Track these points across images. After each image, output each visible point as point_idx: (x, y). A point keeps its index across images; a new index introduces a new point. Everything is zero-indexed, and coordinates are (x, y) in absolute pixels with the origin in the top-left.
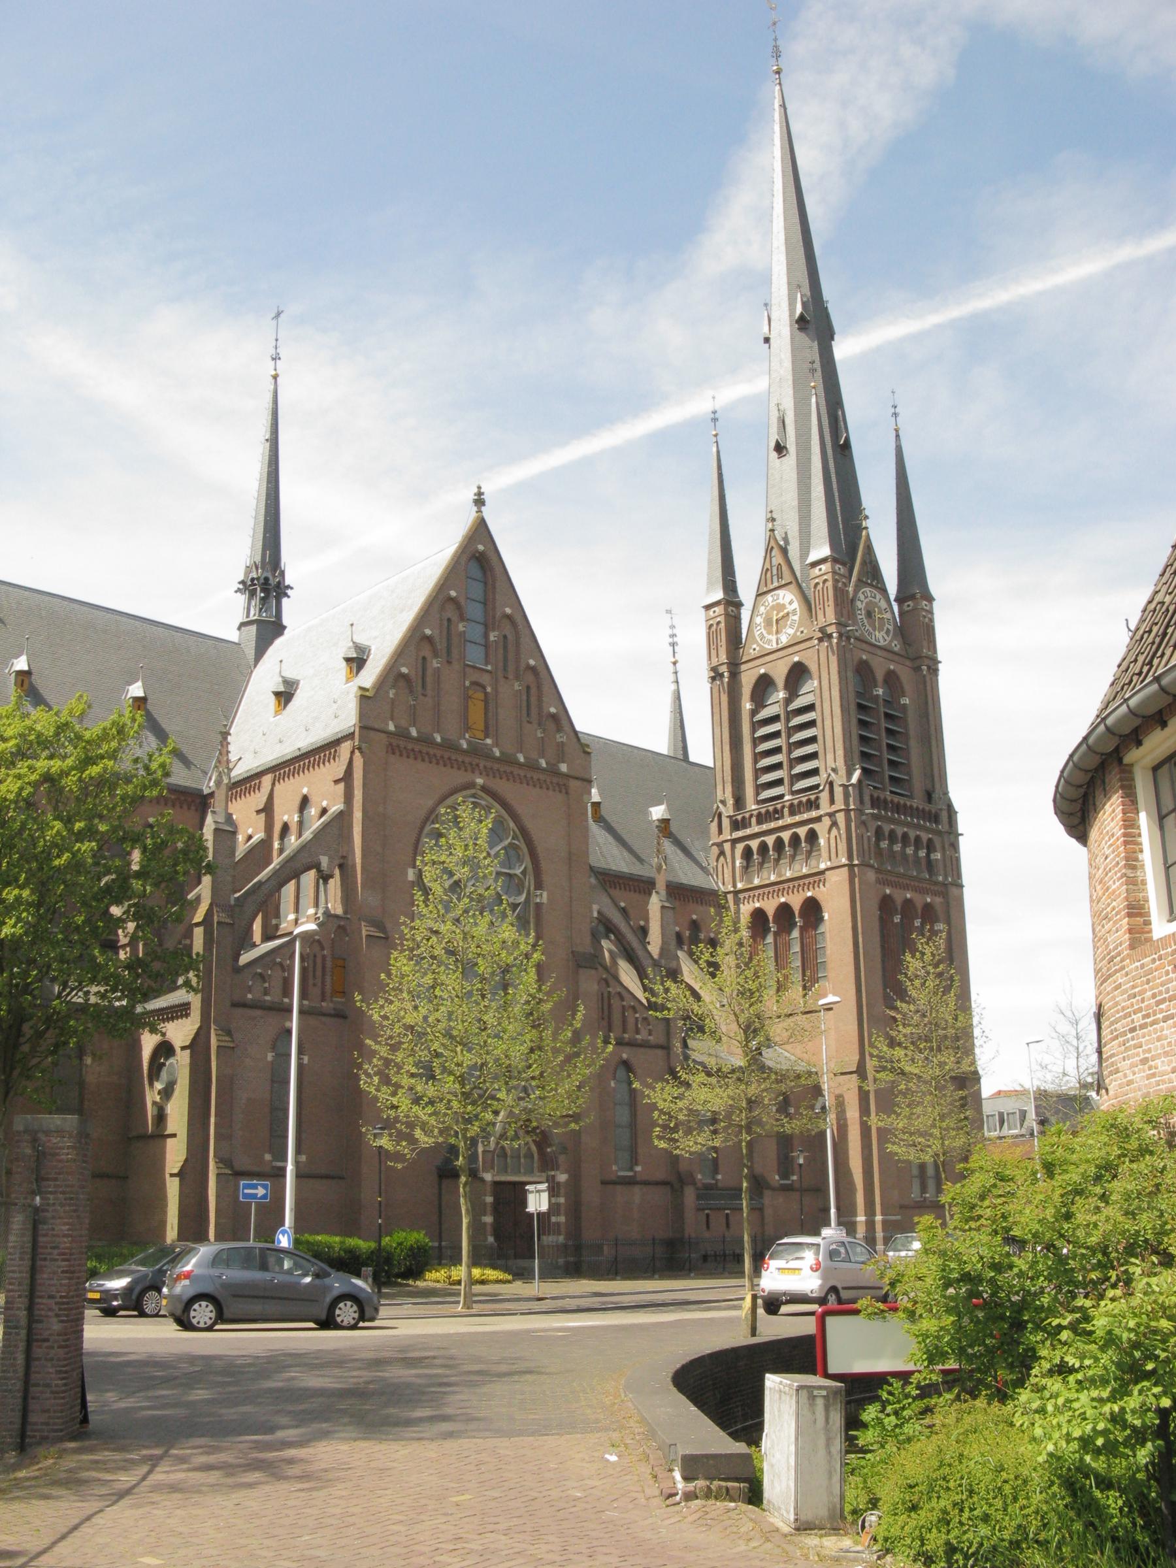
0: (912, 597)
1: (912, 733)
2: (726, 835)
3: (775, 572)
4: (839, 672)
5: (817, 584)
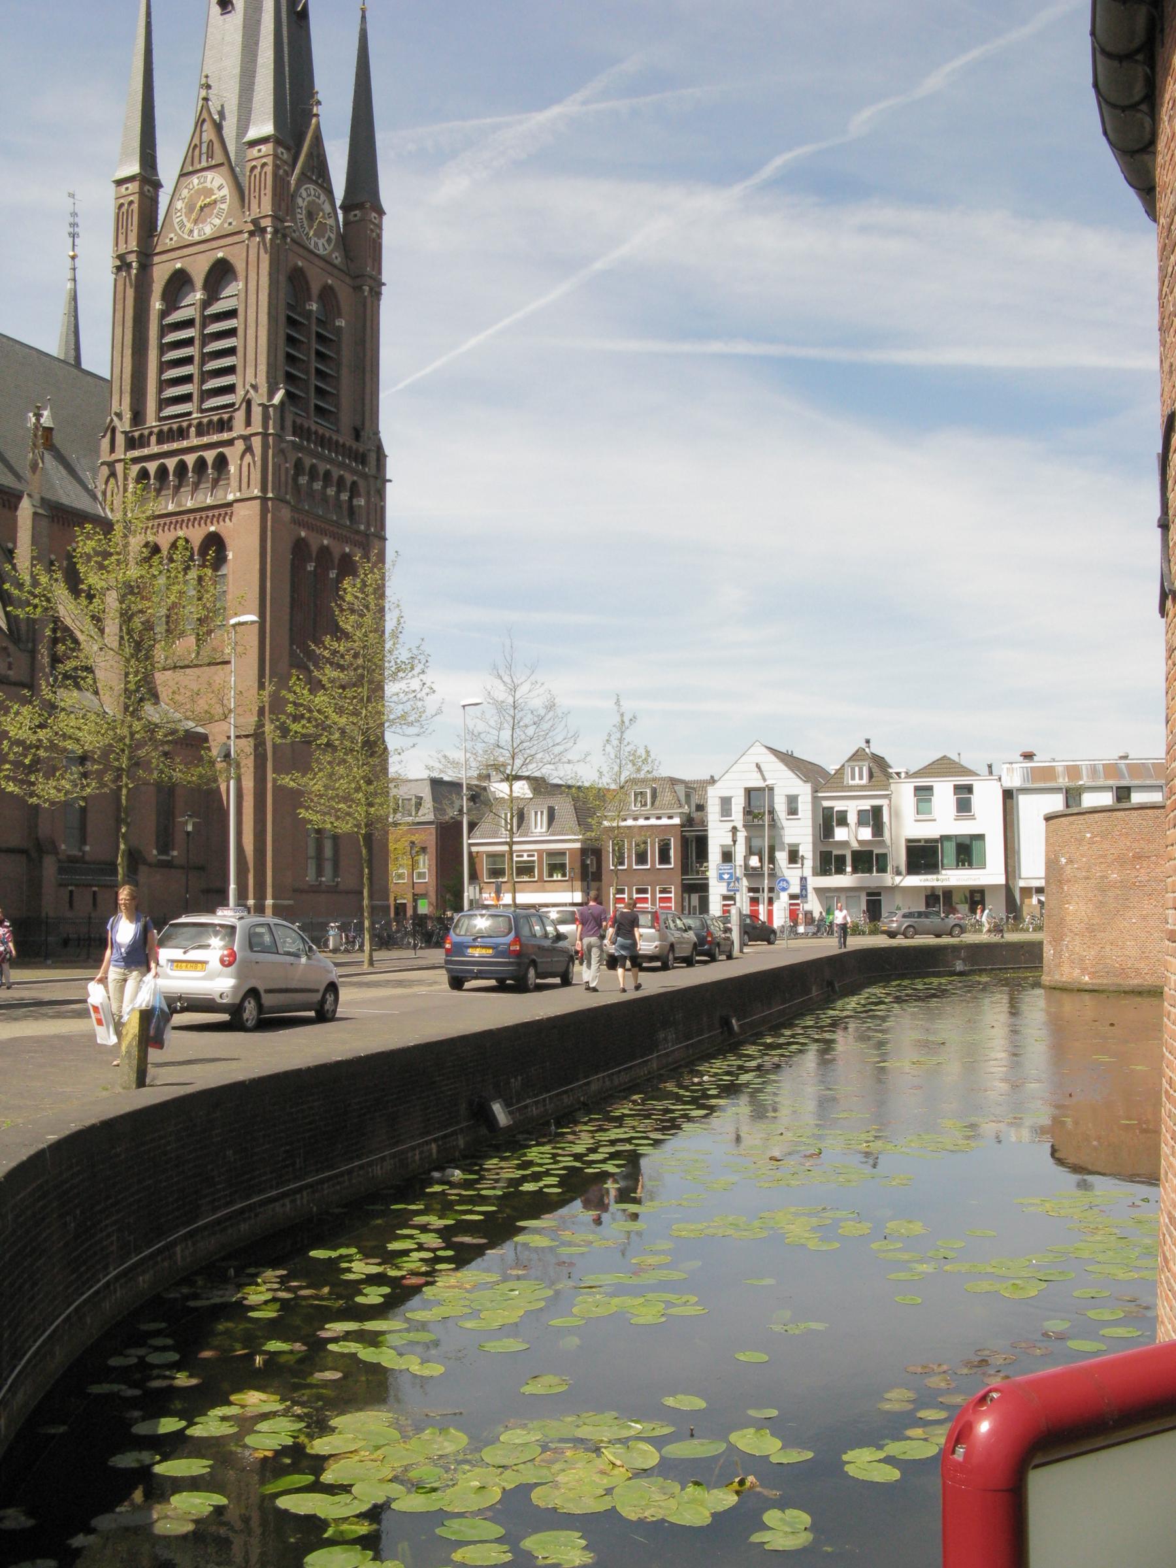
0: (360, 206)
1: (345, 361)
2: (120, 454)
3: (204, 149)
4: (270, 274)
5: (254, 168)
